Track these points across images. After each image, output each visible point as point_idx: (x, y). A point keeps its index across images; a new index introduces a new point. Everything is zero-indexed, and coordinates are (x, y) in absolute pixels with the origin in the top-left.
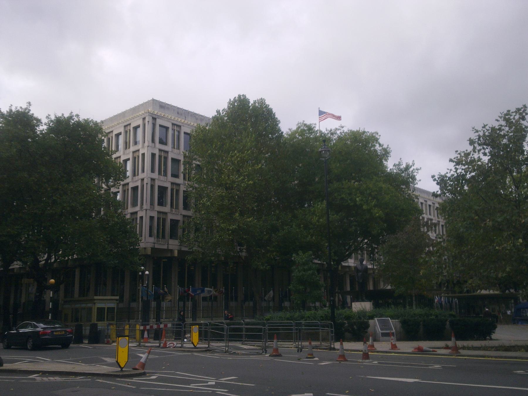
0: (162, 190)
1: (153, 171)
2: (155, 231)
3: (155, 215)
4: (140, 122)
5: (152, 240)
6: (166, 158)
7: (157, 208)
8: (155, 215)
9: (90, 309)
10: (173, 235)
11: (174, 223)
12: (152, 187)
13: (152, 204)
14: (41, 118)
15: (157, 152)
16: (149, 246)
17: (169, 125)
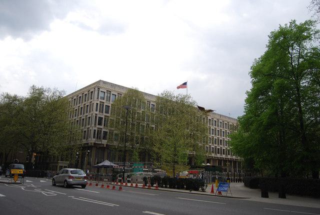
0: (101, 119)
1: (96, 111)
2: (96, 136)
3: (96, 129)
4: (93, 90)
5: (94, 139)
6: (103, 105)
7: (98, 126)
8: (96, 129)
9: (57, 166)
10: (104, 138)
11: (105, 133)
12: (96, 117)
13: (95, 124)
14: (33, 88)
15: (99, 103)
16: (93, 142)
17: (105, 91)
